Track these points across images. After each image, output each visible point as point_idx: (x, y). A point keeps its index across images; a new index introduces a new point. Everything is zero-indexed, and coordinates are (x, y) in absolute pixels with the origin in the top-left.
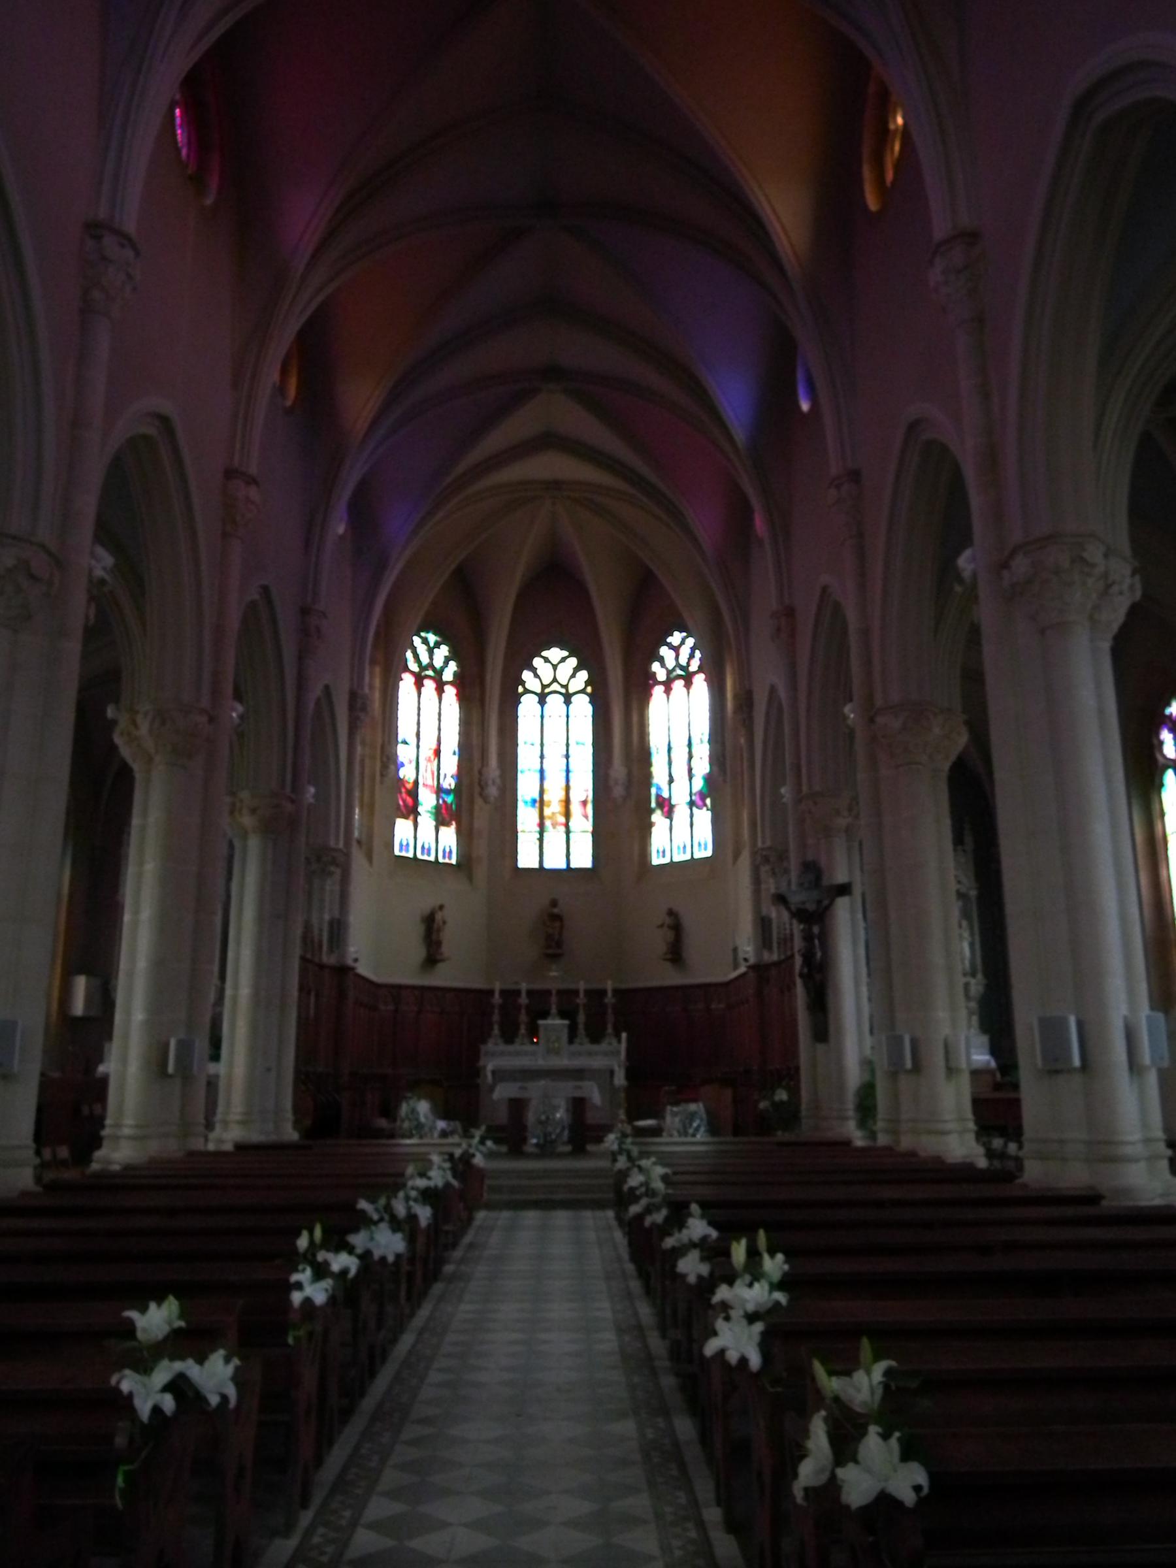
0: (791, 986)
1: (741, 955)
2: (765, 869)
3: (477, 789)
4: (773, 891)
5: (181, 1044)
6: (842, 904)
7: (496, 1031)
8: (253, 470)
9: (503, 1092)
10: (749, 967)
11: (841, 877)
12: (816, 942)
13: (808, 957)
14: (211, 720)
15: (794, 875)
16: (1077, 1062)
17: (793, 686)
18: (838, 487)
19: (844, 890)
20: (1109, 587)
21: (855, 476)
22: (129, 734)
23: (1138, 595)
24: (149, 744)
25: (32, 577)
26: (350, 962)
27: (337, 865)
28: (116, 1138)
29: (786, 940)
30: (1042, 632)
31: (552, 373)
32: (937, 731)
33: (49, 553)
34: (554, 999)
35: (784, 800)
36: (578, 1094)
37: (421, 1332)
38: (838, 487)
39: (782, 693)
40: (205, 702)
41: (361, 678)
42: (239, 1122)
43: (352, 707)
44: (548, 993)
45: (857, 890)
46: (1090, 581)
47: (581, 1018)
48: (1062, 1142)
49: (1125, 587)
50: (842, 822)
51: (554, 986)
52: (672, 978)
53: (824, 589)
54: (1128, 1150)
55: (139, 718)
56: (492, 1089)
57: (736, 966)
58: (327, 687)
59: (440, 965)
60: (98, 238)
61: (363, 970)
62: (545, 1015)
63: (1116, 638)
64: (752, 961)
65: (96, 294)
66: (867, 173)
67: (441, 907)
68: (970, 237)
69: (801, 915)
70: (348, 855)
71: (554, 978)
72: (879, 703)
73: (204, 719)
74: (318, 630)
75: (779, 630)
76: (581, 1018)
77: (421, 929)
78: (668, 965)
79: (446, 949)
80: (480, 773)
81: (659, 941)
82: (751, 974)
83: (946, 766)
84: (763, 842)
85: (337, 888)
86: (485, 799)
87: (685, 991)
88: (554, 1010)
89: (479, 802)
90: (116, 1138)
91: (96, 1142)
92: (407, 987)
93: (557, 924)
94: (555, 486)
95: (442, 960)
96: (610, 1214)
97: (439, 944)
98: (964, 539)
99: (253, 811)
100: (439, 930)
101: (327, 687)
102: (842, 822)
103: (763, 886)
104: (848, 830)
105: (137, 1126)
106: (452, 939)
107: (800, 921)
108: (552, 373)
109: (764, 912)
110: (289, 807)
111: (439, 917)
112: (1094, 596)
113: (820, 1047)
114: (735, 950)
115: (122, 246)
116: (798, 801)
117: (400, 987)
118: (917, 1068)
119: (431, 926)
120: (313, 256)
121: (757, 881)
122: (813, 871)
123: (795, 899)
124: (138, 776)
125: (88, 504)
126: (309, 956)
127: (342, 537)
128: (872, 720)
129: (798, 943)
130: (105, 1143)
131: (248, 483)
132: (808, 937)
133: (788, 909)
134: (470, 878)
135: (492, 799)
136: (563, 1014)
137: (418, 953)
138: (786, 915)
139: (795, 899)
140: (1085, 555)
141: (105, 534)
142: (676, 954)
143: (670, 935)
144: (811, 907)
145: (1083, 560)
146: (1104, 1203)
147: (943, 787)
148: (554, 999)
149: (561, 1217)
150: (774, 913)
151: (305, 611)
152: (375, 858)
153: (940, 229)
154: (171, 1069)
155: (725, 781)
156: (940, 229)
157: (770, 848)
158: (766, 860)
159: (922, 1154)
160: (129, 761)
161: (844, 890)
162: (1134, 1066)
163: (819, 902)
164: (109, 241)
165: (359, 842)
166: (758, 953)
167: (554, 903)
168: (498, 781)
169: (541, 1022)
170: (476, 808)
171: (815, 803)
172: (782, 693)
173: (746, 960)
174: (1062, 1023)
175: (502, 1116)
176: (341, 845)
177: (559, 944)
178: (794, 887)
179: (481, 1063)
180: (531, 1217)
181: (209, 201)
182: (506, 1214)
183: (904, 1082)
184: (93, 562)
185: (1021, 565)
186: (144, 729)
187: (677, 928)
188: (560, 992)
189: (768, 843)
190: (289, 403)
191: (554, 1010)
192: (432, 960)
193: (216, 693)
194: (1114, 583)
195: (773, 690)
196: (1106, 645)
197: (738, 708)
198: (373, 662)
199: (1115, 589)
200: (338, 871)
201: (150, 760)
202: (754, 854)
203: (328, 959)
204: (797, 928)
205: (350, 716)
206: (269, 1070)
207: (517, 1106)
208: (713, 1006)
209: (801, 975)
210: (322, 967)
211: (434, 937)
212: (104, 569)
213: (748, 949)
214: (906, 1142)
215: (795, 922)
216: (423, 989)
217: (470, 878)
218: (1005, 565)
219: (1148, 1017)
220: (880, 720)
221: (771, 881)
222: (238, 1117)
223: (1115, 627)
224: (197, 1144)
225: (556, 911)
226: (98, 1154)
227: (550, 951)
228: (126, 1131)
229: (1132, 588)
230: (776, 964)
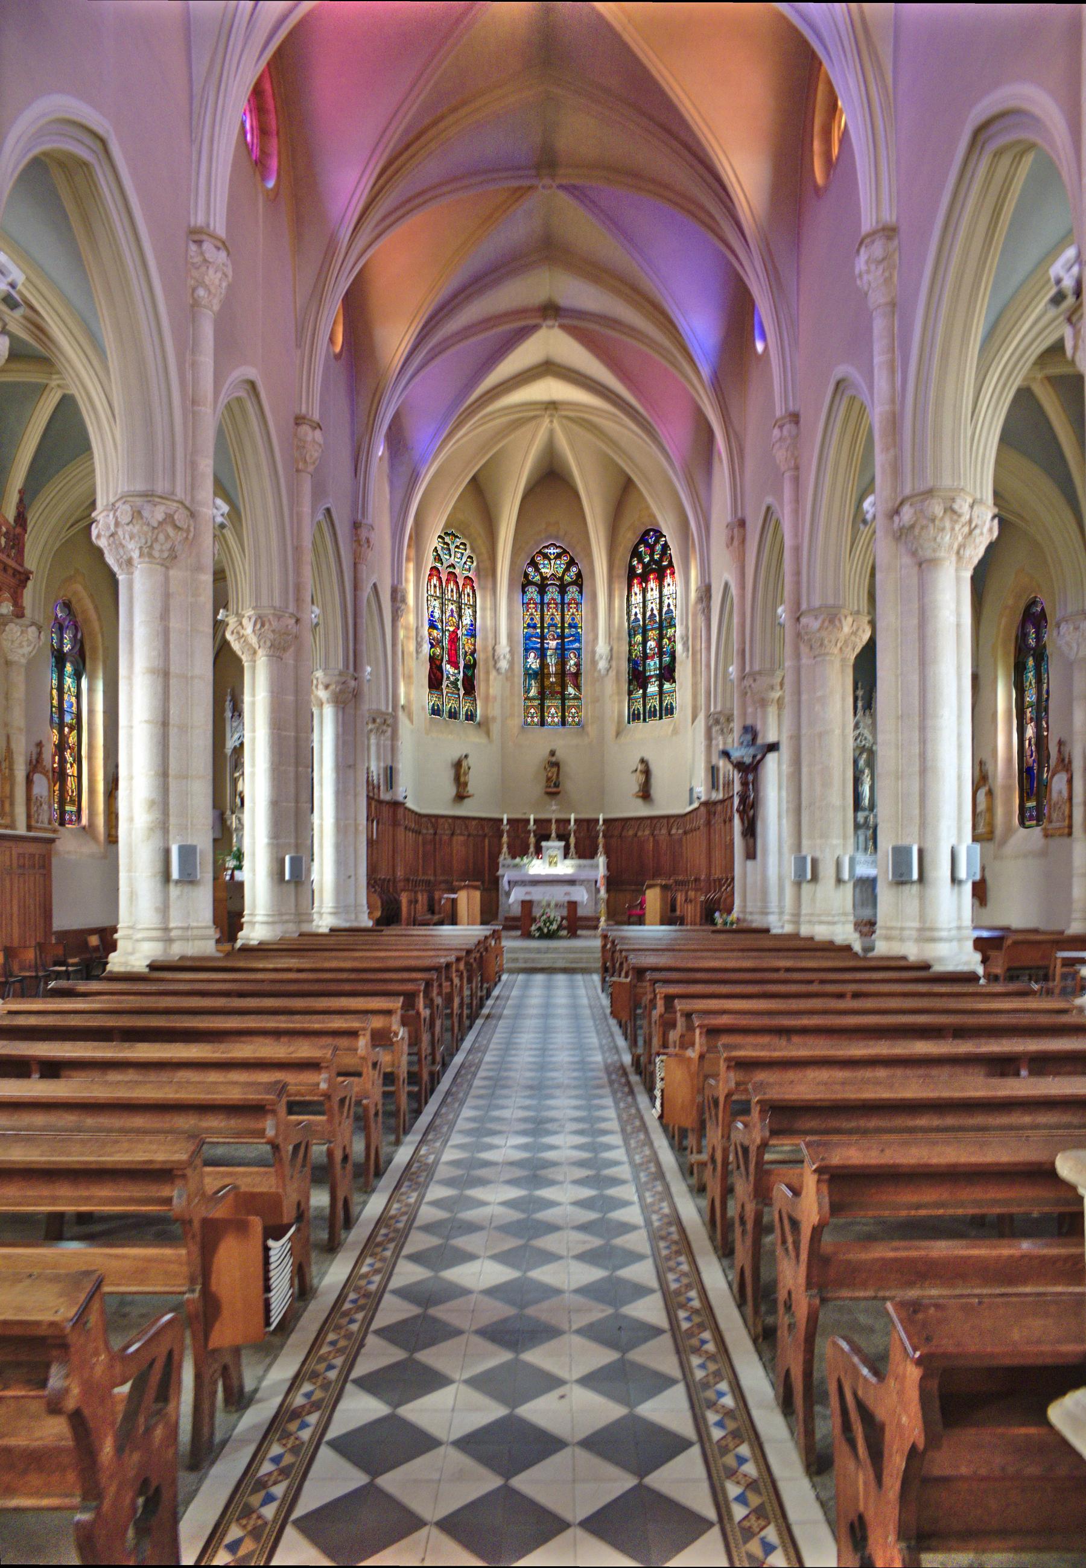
0: (731, 819)
1: (695, 796)
2: (715, 729)
3: (491, 663)
4: (721, 747)
5: (292, 859)
6: (772, 758)
7: (505, 849)
8: (316, 417)
9: (517, 896)
10: (702, 804)
11: (772, 738)
12: (751, 786)
13: (744, 798)
14: (297, 621)
15: (736, 734)
16: (915, 876)
17: (742, 587)
18: (781, 427)
19: (773, 747)
20: (971, 532)
21: (795, 418)
22: (238, 633)
23: (996, 534)
24: (253, 640)
25: (177, 528)
26: (401, 799)
27: (388, 725)
28: (253, 923)
29: (728, 784)
30: (920, 565)
31: (550, 311)
32: (846, 629)
33: (187, 508)
34: (554, 827)
35: (732, 677)
36: (528, 898)
37: (470, 1051)
38: (781, 427)
39: (734, 590)
40: (291, 608)
41: (399, 572)
42: (331, 913)
43: (394, 598)
44: (549, 821)
45: (784, 748)
46: (957, 527)
47: (572, 840)
48: (902, 929)
49: (985, 529)
50: (776, 694)
51: (554, 817)
52: (642, 810)
53: (768, 508)
54: (771, 910)
55: (245, 621)
56: (508, 894)
57: (691, 803)
58: (375, 585)
59: (466, 801)
60: (199, 243)
61: (410, 804)
62: (547, 838)
63: (975, 569)
64: (703, 799)
65: (201, 292)
66: (817, 145)
67: (466, 756)
68: (889, 232)
69: (740, 766)
70: (395, 717)
71: (552, 812)
72: (804, 606)
73: (293, 621)
74: (368, 541)
75: (732, 538)
76: (572, 840)
77: (450, 774)
78: (640, 801)
79: (471, 789)
80: (494, 649)
81: (633, 784)
82: (703, 809)
83: (852, 657)
84: (715, 707)
85: (389, 743)
86: (498, 670)
87: (653, 821)
88: (554, 835)
89: (493, 674)
90: (253, 923)
91: (240, 927)
92: (443, 817)
93: (555, 769)
94: (552, 406)
95: (469, 797)
96: (596, 978)
97: (466, 784)
98: (867, 489)
99: (327, 687)
100: (466, 774)
101: (375, 585)
102: (776, 694)
103: (714, 742)
104: (780, 702)
105: (268, 915)
106: (475, 782)
107: (739, 771)
108: (550, 311)
109: (714, 762)
110: (352, 683)
111: (464, 764)
112: (960, 538)
113: (750, 863)
114: (691, 790)
115: (218, 249)
116: (743, 678)
117: (437, 817)
118: (815, 878)
119: (459, 768)
120: (354, 230)
121: (709, 737)
122: (751, 732)
123: (736, 755)
124: (246, 665)
125: (207, 465)
126: (371, 794)
127: (381, 458)
128: (798, 619)
129: (737, 787)
130: (245, 926)
131: (314, 428)
132: (744, 784)
133: (732, 763)
134: (488, 733)
135: (503, 671)
136: (560, 837)
137: (451, 790)
138: (730, 767)
139: (736, 755)
140: (956, 507)
141: (221, 489)
142: (645, 794)
143: (642, 778)
144: (748, 760)
145: (954, 511)
146: (931, 970)
147: (850, 672)
148: (554, 827)
149: (561, 979)
150: (722, 763)
151: (356, 526)
152: (415, 718)
153: (867, 224)
154: (287, 877)
155: (687, 657)
156: (867, 224)
157: (720, 713)
158: (717, 722)
159: (818, 938)
160: (239, 653)
161: (773, 747)
162: (954, 880)
163: (754, 757)
164: (207, 246)
165: (403, 707)
166: (708, 792)
167: (553, 753)
168: (508, 656)
169: (544, 844)
170: (492, 677)
171: (755, 680)
172: (734, 590)
173: (699, 798)
174: (908, 851)
175: (516, 911)
176: (390, 710)
177: (557, 785)
178: (736, 745)
179: (500, 872)
180: (539, 978)
181: (271, 184)
182: (521, 977)
183: (805, 887)
184: (215, 511)
185: (907, 514)
186: (248, 630)
187: (647, 773)
188: (557, 821)
189: (719, 709)
190: (338, 349)
191: (554, 835)
192: (460, 797)
193: (298, 600)
194: (976, 526)
195: (726, 586)
196: (968, 574)
197: (700, 600)
198: (408, 559)
199: (977, 531)
200: (389, 730)
201: (255, 652)
202: (708, 716)
203: (385, 796)
204: (737, 777)
205: (393, 606)
206: (350, 877)
207: (527, 905)
208: (673, 831)
209: (738, 810)
210: (380, 802)
211: (462, 779)
212: (222, 515)
213: (701, 790)
214: (805, 931)
215: (736, 772)
216: (456, 818)
217: (488, 733)
218: (897, 512)
219: (968, 847)
220: (804, 620)
221: (720, 738)
222: (329, 910)
223: (976, 561)
224: (306, 928)
225: (554, 759)
226: (240, 934)
227: (550, 790)
228: (259, 918)
229: (991, 530)
230: (722, 801)
